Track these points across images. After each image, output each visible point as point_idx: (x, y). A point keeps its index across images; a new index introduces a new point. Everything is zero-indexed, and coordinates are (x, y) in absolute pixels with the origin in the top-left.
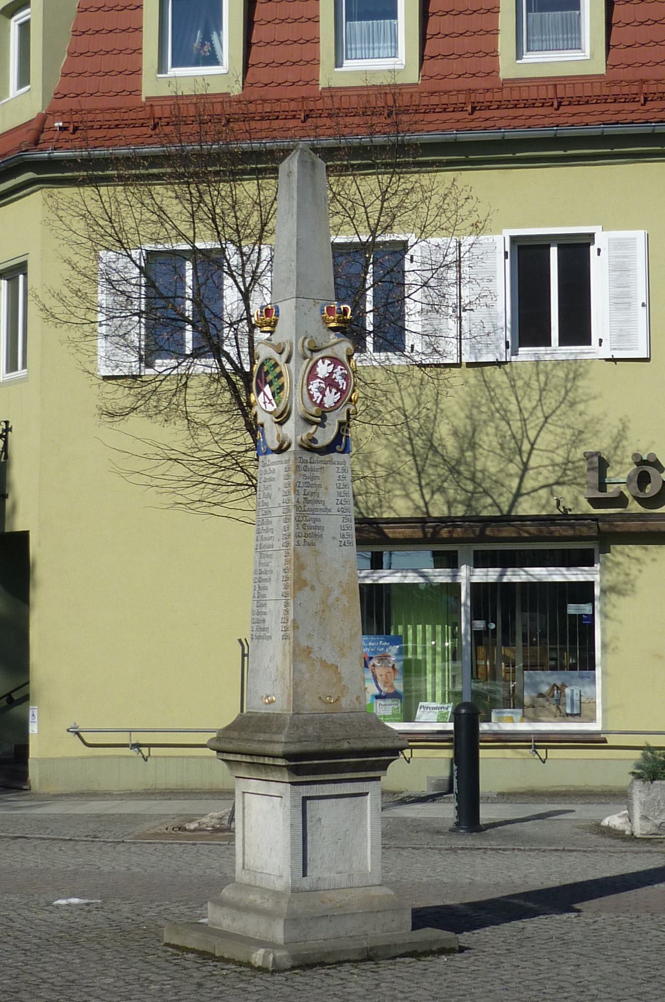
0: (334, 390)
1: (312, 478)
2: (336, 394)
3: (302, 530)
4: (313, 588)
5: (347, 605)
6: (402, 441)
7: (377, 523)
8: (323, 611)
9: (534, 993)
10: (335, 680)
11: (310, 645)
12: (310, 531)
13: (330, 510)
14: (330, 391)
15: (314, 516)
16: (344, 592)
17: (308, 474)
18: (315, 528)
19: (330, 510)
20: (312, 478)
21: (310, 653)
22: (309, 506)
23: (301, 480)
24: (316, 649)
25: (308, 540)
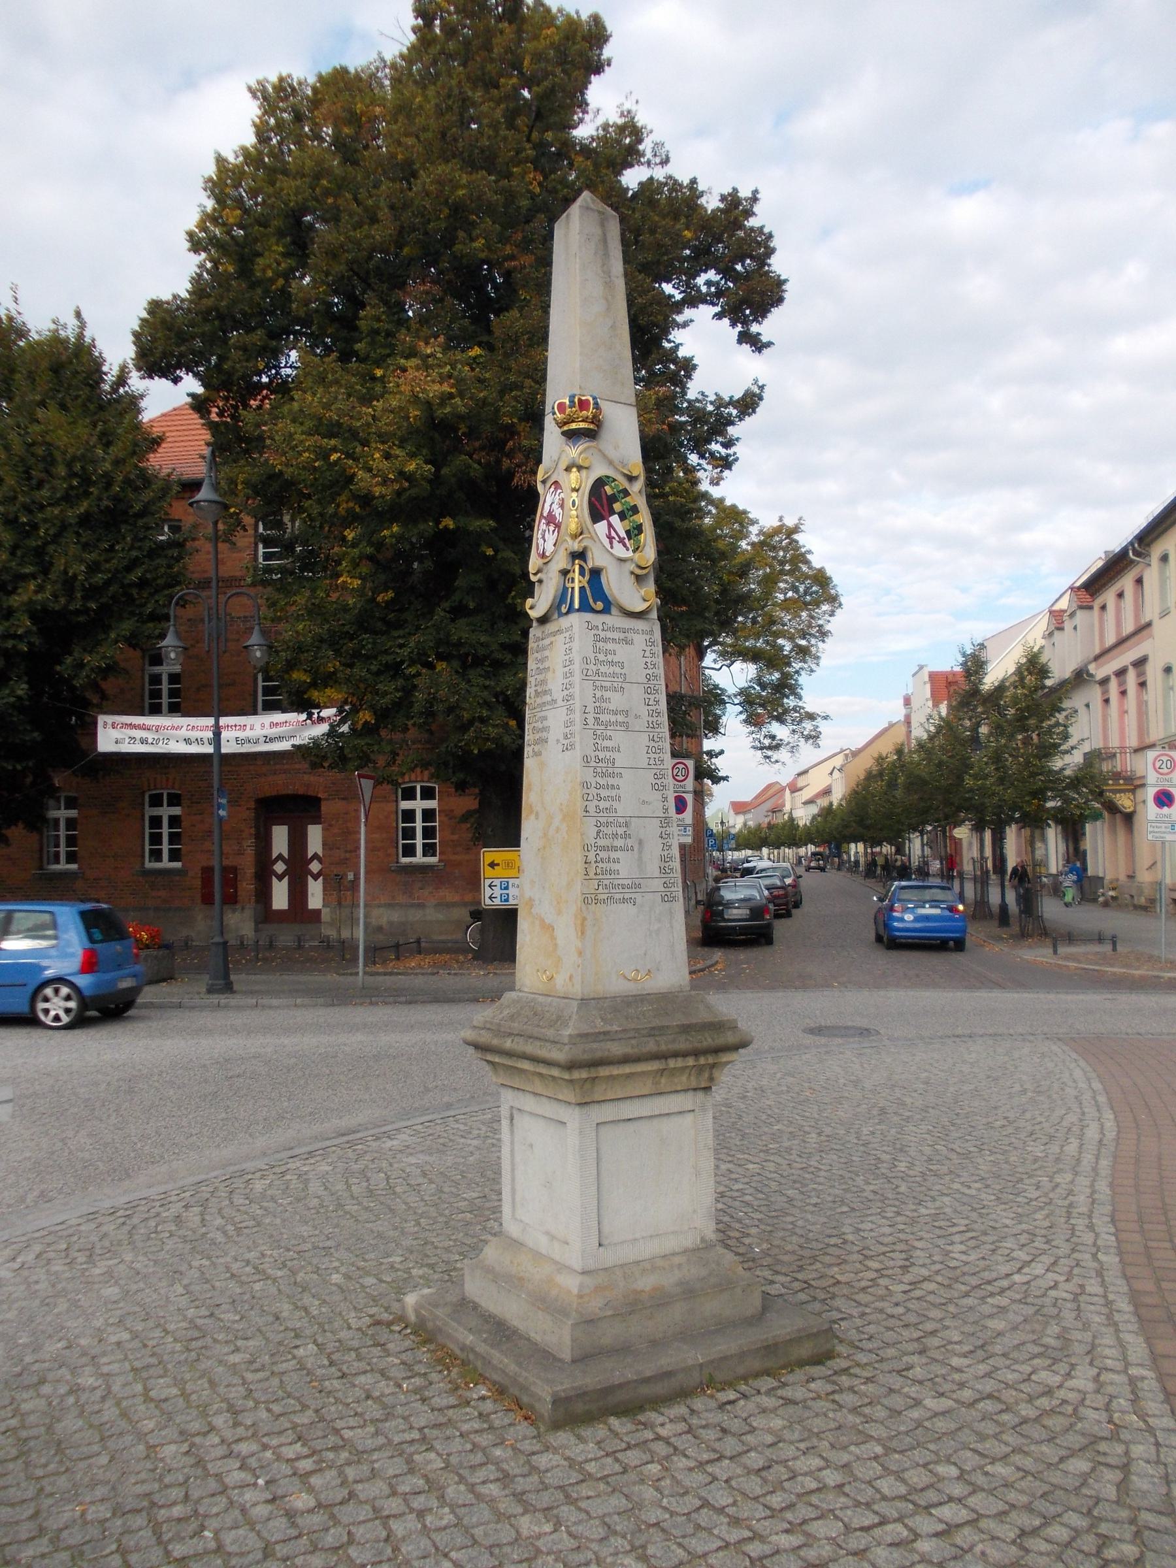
4: (537, 814)
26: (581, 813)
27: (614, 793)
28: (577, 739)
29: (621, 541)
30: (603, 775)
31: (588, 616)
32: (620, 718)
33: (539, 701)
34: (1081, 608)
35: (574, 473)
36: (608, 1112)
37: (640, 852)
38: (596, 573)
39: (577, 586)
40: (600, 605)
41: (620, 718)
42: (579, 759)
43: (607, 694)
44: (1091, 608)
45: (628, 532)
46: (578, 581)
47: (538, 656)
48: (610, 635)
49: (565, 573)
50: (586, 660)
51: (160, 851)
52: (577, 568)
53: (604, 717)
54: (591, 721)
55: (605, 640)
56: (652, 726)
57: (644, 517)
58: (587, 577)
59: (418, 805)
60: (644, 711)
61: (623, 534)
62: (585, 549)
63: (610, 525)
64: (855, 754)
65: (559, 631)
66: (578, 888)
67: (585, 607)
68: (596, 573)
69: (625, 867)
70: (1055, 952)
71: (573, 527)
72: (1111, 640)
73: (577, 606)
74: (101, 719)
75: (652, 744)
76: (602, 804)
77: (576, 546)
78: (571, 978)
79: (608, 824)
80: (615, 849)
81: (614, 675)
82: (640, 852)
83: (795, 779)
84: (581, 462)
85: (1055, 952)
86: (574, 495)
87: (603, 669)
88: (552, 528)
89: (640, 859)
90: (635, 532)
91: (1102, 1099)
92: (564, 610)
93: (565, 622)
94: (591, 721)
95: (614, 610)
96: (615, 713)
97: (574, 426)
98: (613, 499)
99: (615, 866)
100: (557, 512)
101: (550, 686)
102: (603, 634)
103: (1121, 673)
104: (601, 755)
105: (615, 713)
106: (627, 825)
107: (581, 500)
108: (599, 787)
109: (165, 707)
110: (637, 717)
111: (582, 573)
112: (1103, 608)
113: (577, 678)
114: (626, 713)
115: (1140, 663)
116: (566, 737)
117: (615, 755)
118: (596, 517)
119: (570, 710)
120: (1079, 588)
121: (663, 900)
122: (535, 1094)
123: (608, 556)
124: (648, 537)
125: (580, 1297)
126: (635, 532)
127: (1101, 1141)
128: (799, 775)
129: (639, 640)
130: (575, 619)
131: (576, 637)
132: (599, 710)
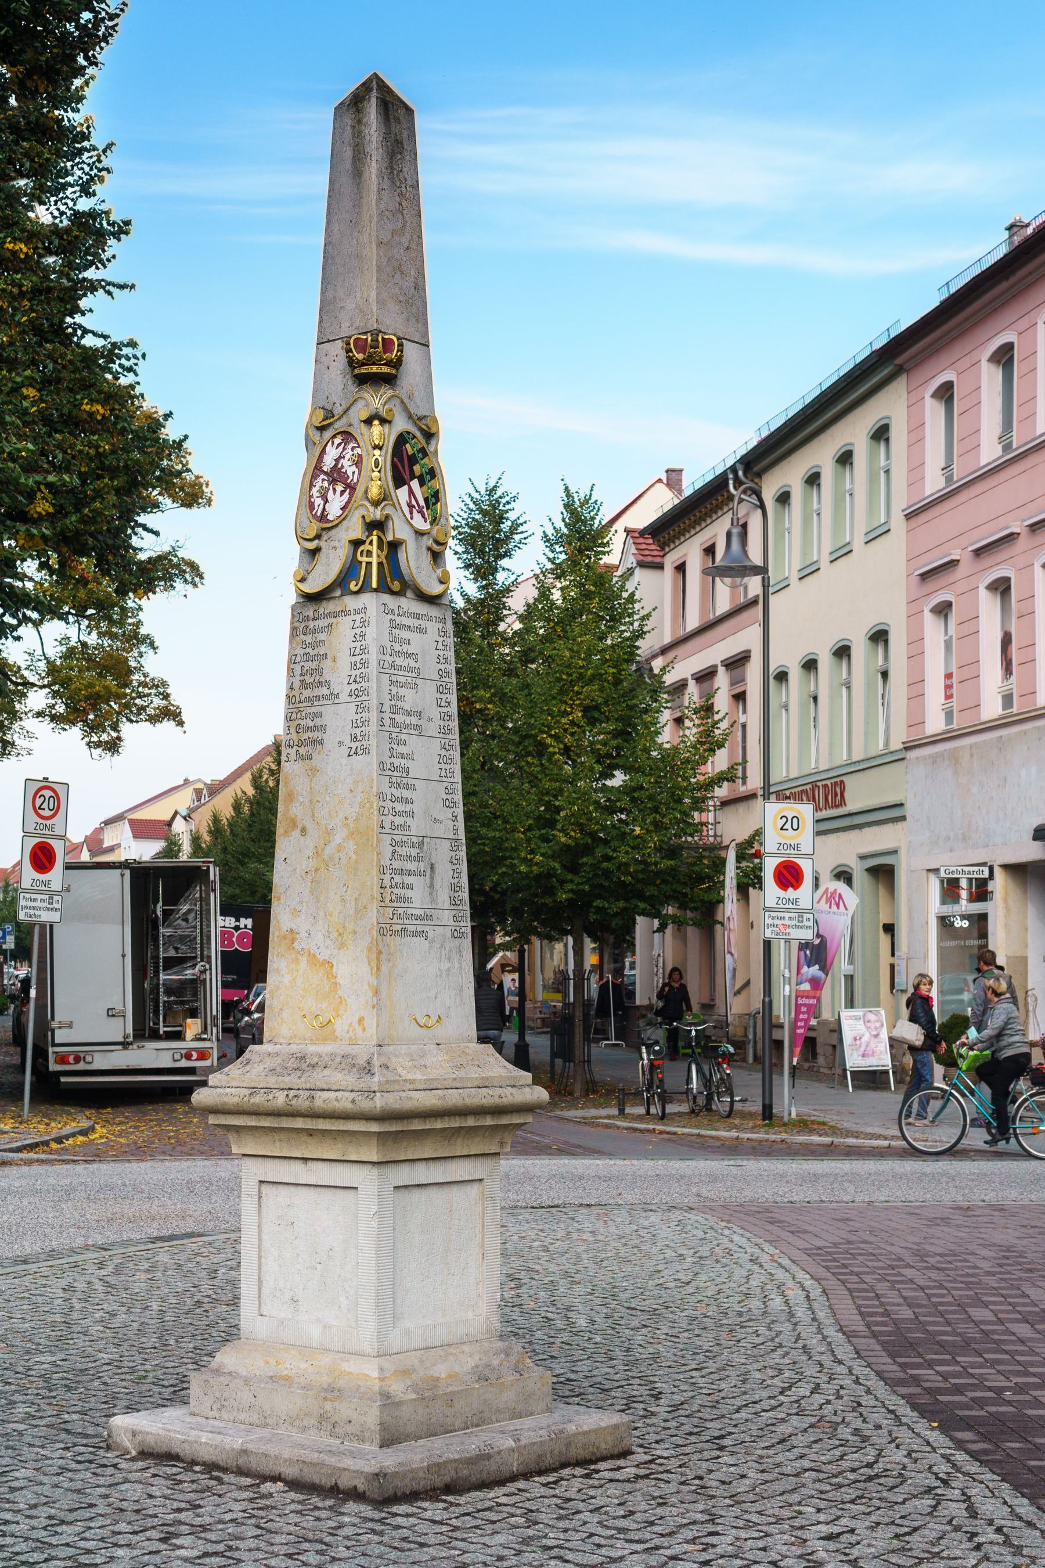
0: (339, 488)
1: (315, 645)
2: (342, 493)
3: (294, 736)
4: (304, 831)
5: (354, 857)
6: (958, 1025)
7: (166, 558)
8: (316, 870)
9: (845, 1465)
10: (327, 989)
11: (294, 927)
12: (305, 736)
13: (337, 696)
14: (334, 490)
15: (313, 710)
16: (351, 834)
17: (308, 639)
18: (316, 728)
19: (337, 696)
20: (315, 645)
21: (293, 940)
22: (307, 693)
23: (300, 651)
24: (304, 935)
25: (302, 751)
26: (376, 828)
27: (408, 807)
28: (373, 741)
29: (421, 512)
30: (398, 786)
31: (386, 598)
32: (414, 720)
34: (642, 565)
35: (377, 428)
36: (405, 1175)
37: (432, 878)
38: (394, 546)
39: (374, 560)
40: (396, 586)
41: (414, 720)
42: (375, 766)
43: (402, 692)
44: (660, 567)
45: (426, 500)
46: (374, 556)
48: (405, 621)
49: (357, 543)
50: (382, 649)
52: (375, 538)
53: (400, 718)
54: (387, 722)
55: (400, 627)
56: (445, 731)
58: (385, 551)
60: (435, 713)
61: (422, 503)
62: (387, 517)
63: (411, 492)
64: (215, 789)
65: (345, 612)
66: (372, 915)
67: (383, 588)
68: (394, 546)
69: (417, 895)
70: (622, 1111)
71: (374, 492)
72: (693, 622)
73: (374, 585)
75: (443, 752)
76: (398, 820)
77: (377, 514)
78: (361, 1020)
79: (402, 844)
80: (409, 873)
81: (408, 669)
82: (432, 878)
83: (99, 831)
84: (384, 415)
85: (622, 1111)
86: (377, 452)
87: (399, 661)
88: (339, 488)
89: (431, 886)
91: (786, 1262)
92: (353, 586)
93: (351, 603)
94: (387, 722)
95: (409, 594)
96: (409, 713)
97: (374, 369)
98: (413, 460)
99: (409, 893)
100: (350, 470)
101: (327, 676)
102: (399, 620)
103: (705, 676)
104: (397, 762)
105: (409, 713)
106: (421, 845)
107: (384, 457)
108: (395, 799)
110: (430, 720)
111: (380, 547)
112: (681, 568)
113: (373, 670)
114: (418, 714)
115: (737, 663)
116: (355, 739)
117: (409, 763)
118: (399, 481)
119: (361, 708)
120: (642, 533)
121: (453, 936)
123: (407, 528)
125: (381, 1379)
127: (808, 1297)
128: (107, 823)
129: (433, 628)
130: (368, 600)
131: (373, 621)
132: (395, 710)
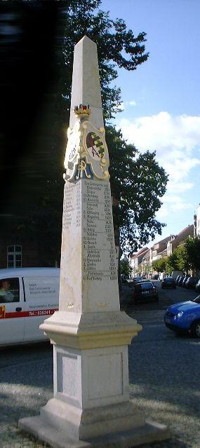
27: (94, 241)
29: (97, 154)
33: (68, 209)
40: (89, 176)
46: (83, 168)
47: (68, 194)
51: (17, 259)
57: (105, 146)
59: (15, 254)
60: (104, 213)
74: (75, 331)
90: (102, 151)
94: (86, 216)
98: (94, 140)
109: (15, 265)
122: (112, 396)
124: (106, 153)
126: (102, 151)
